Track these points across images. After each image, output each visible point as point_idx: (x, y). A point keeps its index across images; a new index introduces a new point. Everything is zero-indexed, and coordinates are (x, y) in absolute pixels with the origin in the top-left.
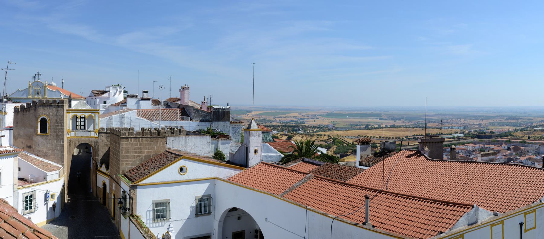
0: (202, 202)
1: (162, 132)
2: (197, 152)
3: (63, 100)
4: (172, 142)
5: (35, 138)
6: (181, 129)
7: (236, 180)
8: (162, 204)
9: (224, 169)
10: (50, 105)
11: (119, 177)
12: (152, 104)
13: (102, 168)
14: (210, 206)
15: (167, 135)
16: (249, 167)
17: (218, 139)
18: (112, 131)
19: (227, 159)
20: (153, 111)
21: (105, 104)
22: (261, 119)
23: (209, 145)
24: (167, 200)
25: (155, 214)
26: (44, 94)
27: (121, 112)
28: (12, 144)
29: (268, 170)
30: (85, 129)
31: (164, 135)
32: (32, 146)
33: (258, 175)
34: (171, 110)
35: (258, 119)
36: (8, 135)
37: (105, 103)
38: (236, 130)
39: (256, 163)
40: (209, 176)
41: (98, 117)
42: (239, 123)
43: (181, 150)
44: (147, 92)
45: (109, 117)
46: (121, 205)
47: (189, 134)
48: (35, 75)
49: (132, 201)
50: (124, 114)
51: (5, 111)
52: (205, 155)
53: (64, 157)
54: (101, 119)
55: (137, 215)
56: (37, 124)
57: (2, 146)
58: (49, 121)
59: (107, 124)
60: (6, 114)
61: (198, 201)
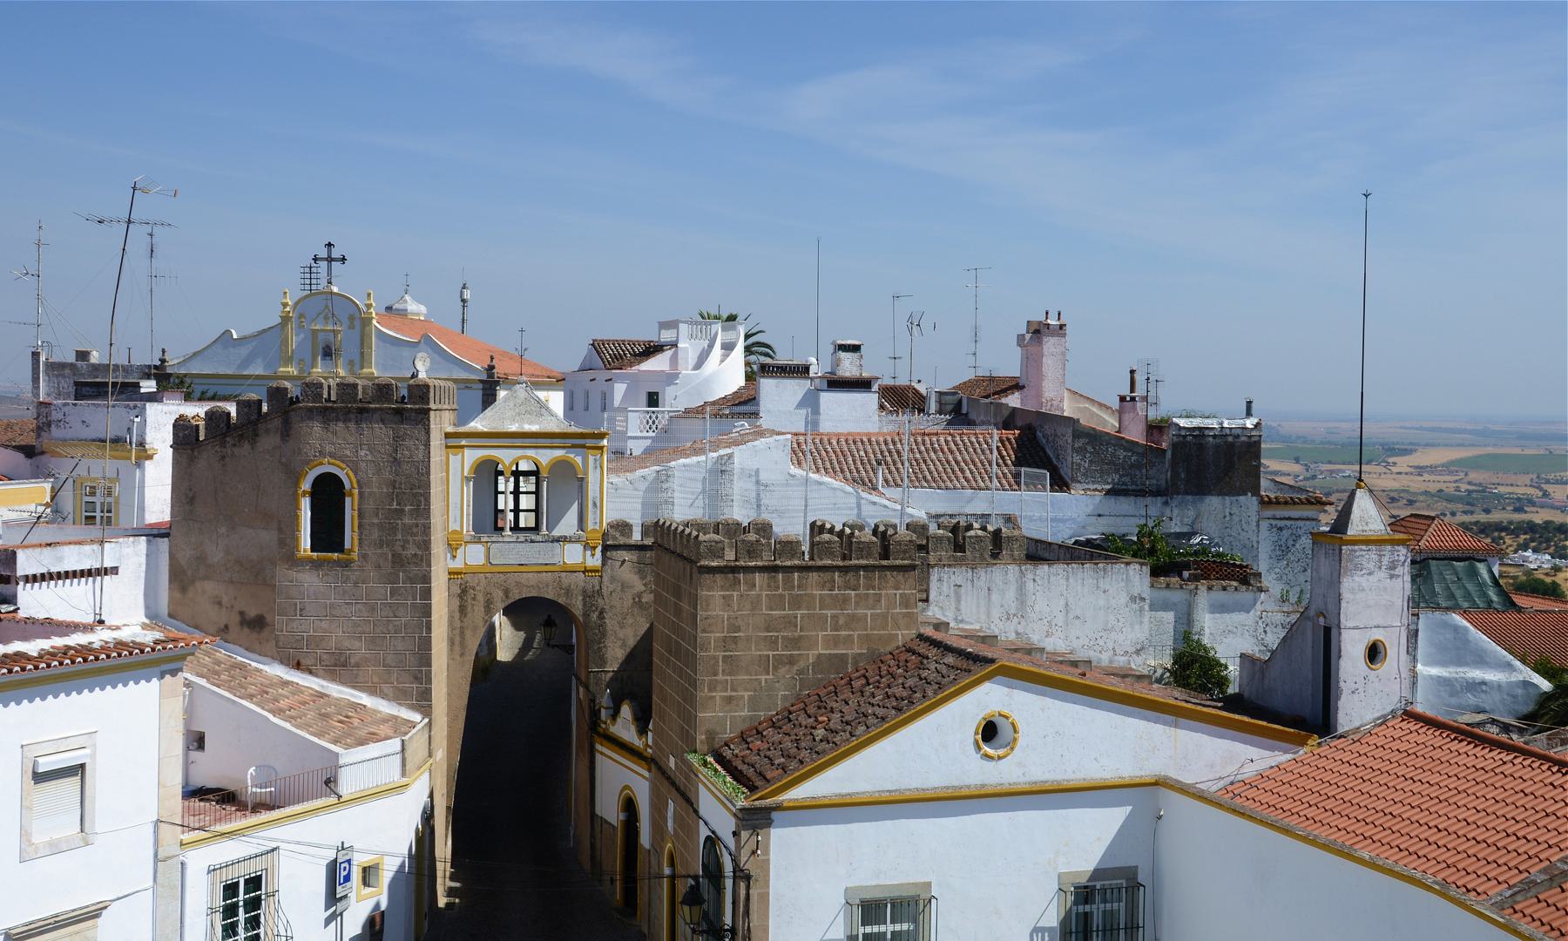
0: (1094, 906)
1: (899, 543)
2: (1076, 644)
3: (427, 387)
4: (952, 594)
5: (284, 575)
6: (1004, 530)
7: (1265, 798)
8: (893, 906)
9: (1205, 738)
10: (361, 411)
11: (690, 766)
12: (882, 407)
15: (932, 559)
16: (1340, 730)
19: (1232, 689)
20: (881, 439)
22: (1464, 487)
26: (362, 353)
28: (163, 607)
29: (1437, 754)
30: (537, 529)
31: (910, 558)
32: (268, 618)
33: (1383, 779)
34: (968, 435)
35: (1450, 489)
37: (653, 400)
39: (1377, 715)
40: (1127, 770)
41: (601, 468)
42: (1308, 507)
45: (658, 468)
46: (696, 909)
47: (1041, 553)
48: (315, 259)
49: (748, 888)
50: (730, 456)
51: (141, 444)
52: (1121, 661)
53: (430, 672)
54: (614, 479)
56: (297, 507)
57: (101, 622)
58: (356, 492)
60: (150, 457)
61: (1071, 898)
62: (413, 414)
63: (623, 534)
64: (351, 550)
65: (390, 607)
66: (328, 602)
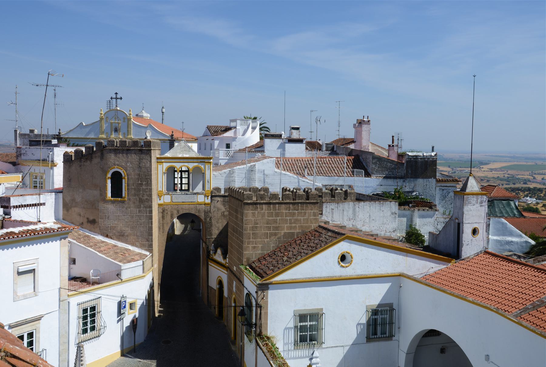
0: (378, 316)
1: (312, 195)
2: (373, 229)
3: (150, 142)
4: (331, 212)
6: (348, 190)
7: (437, 280)
9: (417, 260)
10: (128, 150)
11: (241, 270)
12: (307, 149)
13: (217, 254)
14: (391, 323)
15: (324, 200)
16: (463, 258)
17: (412, 209)
18: (231, 193)
20: (306, 160)
21: (229, 148)
22: (506, 176)
23: (395, 217)
24: (318, 309)
25: (299, 334)
27: (250, 162)
29: (496, 265)
30: (188, 190)
31: (316, 200)
32: (97, 220)
33: (477, 274)
34: (336, 158)
35: (501, 176)
36: (53, 202)
37: (228, 146)
38: (446, 194)
41: (210, 169)
43: (346, 225)
44: (298, 129)
45: (230, 169)
46: (243, 317)
47: (361, 198)
48: (111, 98)
49: (261, 310)
50: (255, 165)
51: (53, 161)
52: (388, 234)
53: (152, 238)
54: (215, 173)
55: (269, 335)
56: (106, 183)
58: (126, 177)
59: (225, 182)
60: (56, 166)
61: (370, 314)
62: (146, 151)
63: (218, 192)
64: (125, 197)
65: (138, 216)
66: (117, 214)
